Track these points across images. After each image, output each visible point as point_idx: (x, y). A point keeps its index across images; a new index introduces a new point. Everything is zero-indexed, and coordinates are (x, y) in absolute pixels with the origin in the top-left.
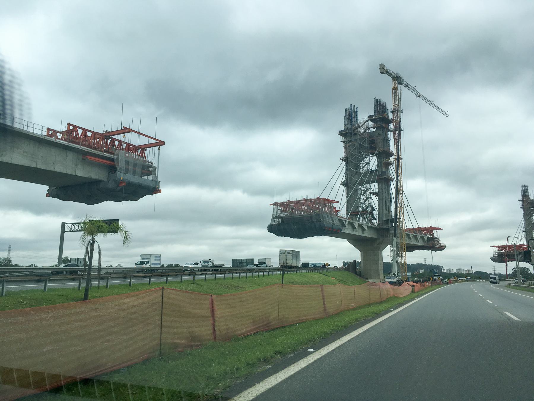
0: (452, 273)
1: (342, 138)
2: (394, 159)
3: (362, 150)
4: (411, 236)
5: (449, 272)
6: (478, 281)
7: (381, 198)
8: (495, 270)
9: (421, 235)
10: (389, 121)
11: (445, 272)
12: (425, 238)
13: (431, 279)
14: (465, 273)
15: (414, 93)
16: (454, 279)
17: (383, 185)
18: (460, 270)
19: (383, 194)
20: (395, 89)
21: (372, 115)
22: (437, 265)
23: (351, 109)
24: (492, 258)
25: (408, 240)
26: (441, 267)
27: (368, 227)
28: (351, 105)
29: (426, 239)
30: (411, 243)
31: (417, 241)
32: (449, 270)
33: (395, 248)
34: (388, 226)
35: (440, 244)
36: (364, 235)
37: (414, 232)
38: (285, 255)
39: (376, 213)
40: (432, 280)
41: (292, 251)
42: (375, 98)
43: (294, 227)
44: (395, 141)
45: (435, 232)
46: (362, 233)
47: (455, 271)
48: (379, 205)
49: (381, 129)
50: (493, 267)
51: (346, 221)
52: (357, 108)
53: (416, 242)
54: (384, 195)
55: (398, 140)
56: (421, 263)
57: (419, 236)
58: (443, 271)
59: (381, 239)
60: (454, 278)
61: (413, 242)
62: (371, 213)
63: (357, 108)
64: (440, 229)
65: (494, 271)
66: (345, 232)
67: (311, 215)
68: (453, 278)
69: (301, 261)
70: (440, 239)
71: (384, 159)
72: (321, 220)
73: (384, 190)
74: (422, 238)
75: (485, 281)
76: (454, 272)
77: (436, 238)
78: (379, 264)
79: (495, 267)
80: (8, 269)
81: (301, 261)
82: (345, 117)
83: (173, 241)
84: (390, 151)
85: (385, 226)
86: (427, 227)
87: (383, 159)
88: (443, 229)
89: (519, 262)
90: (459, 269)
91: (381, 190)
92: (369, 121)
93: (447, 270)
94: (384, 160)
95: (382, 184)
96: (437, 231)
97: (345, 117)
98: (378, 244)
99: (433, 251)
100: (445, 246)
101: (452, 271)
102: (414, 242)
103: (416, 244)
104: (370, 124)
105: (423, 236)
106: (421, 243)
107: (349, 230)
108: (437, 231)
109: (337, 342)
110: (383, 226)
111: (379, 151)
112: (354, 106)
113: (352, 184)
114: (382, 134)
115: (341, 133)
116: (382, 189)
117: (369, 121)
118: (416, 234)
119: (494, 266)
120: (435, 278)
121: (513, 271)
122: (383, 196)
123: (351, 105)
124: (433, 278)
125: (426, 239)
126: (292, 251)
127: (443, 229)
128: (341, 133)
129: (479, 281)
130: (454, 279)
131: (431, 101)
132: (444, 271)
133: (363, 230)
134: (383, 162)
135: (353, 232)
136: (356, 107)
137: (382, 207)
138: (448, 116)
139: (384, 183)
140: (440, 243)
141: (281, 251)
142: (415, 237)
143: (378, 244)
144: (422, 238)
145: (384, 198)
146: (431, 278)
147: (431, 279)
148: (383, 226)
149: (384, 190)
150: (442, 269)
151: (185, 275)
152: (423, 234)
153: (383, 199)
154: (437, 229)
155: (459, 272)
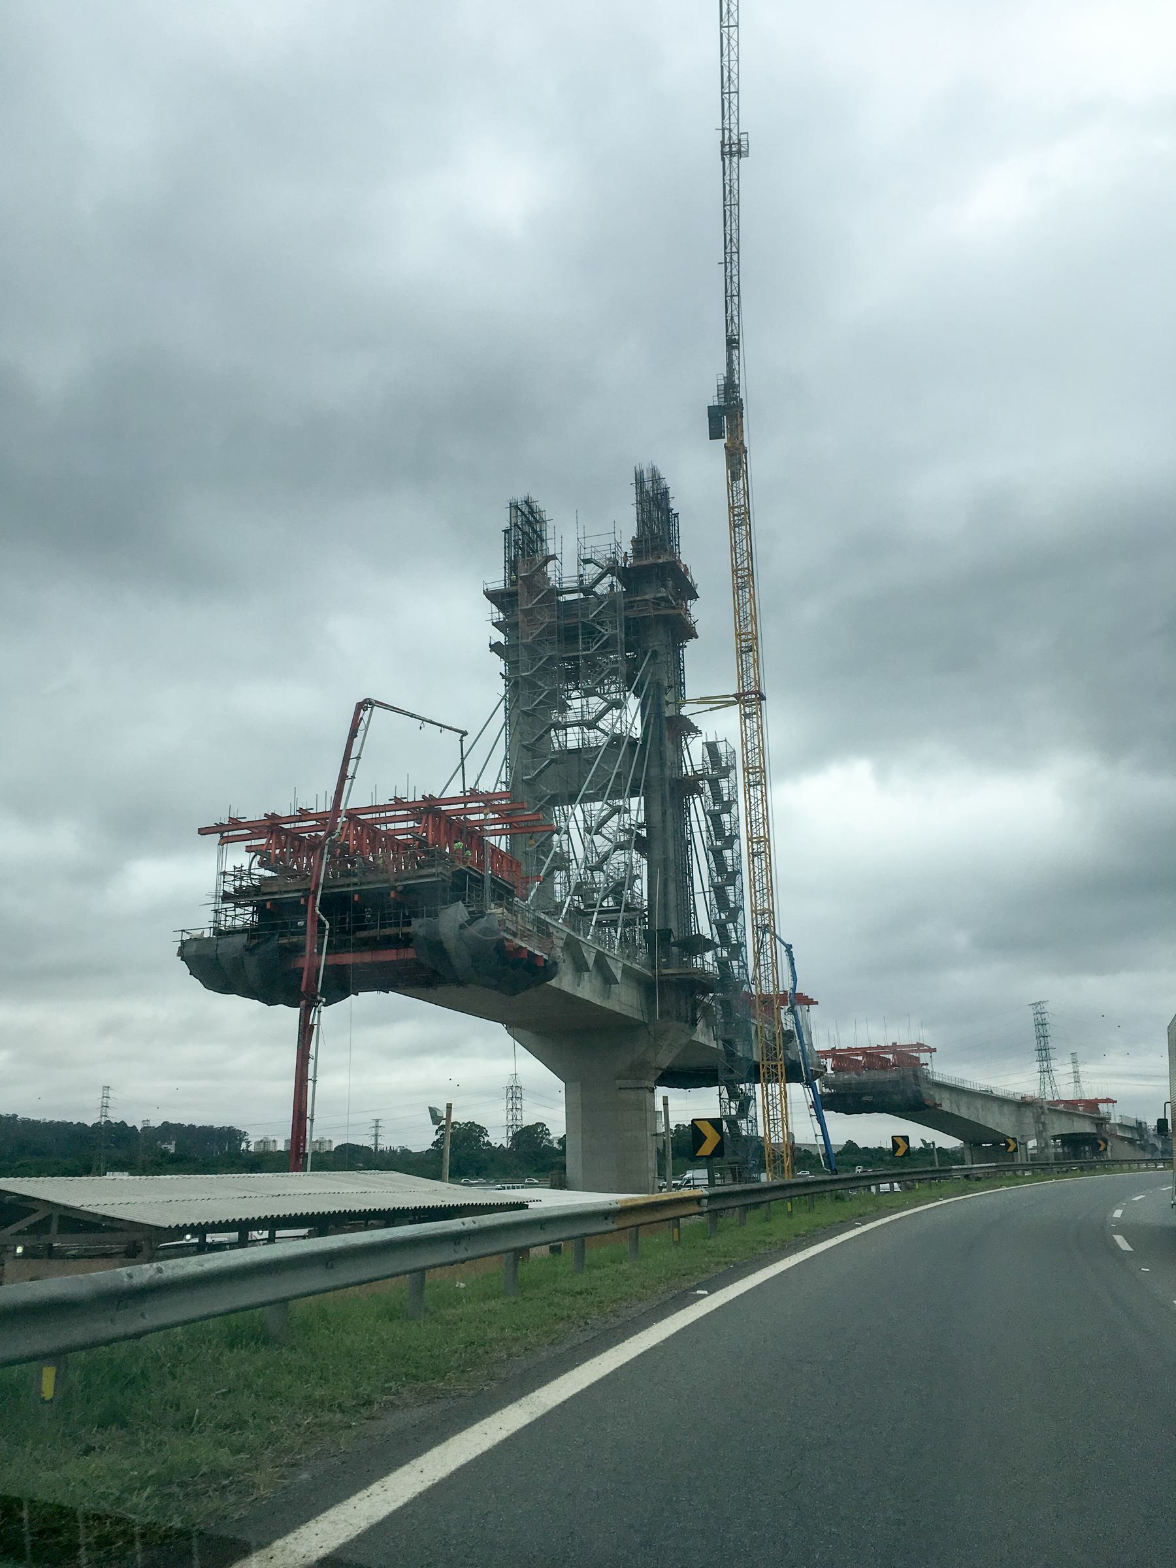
2: (733, 696)
5: (320, 1148)
8: (379, 1133)
11: (252, 1149)
13: (1100, 1145)
22: (230, 1128)
27: (626, 971)
32: (264, 1142)
50: (374, 1125)
56: (177, 1122)
58: (244, 1145)
76: (278, 1149)
79: (380, 1124)
80: (984, 1167)
82: (506, 531)
93: (258, 1143)
97: (506, 531)
101: (272, 1144)
109: (485, 1424)
119: (377, 1121)
121: (438, 1137)
133: (608, 979)
147: (1100, 1145)
150: (241, 1140)
151: (1121, 1162)
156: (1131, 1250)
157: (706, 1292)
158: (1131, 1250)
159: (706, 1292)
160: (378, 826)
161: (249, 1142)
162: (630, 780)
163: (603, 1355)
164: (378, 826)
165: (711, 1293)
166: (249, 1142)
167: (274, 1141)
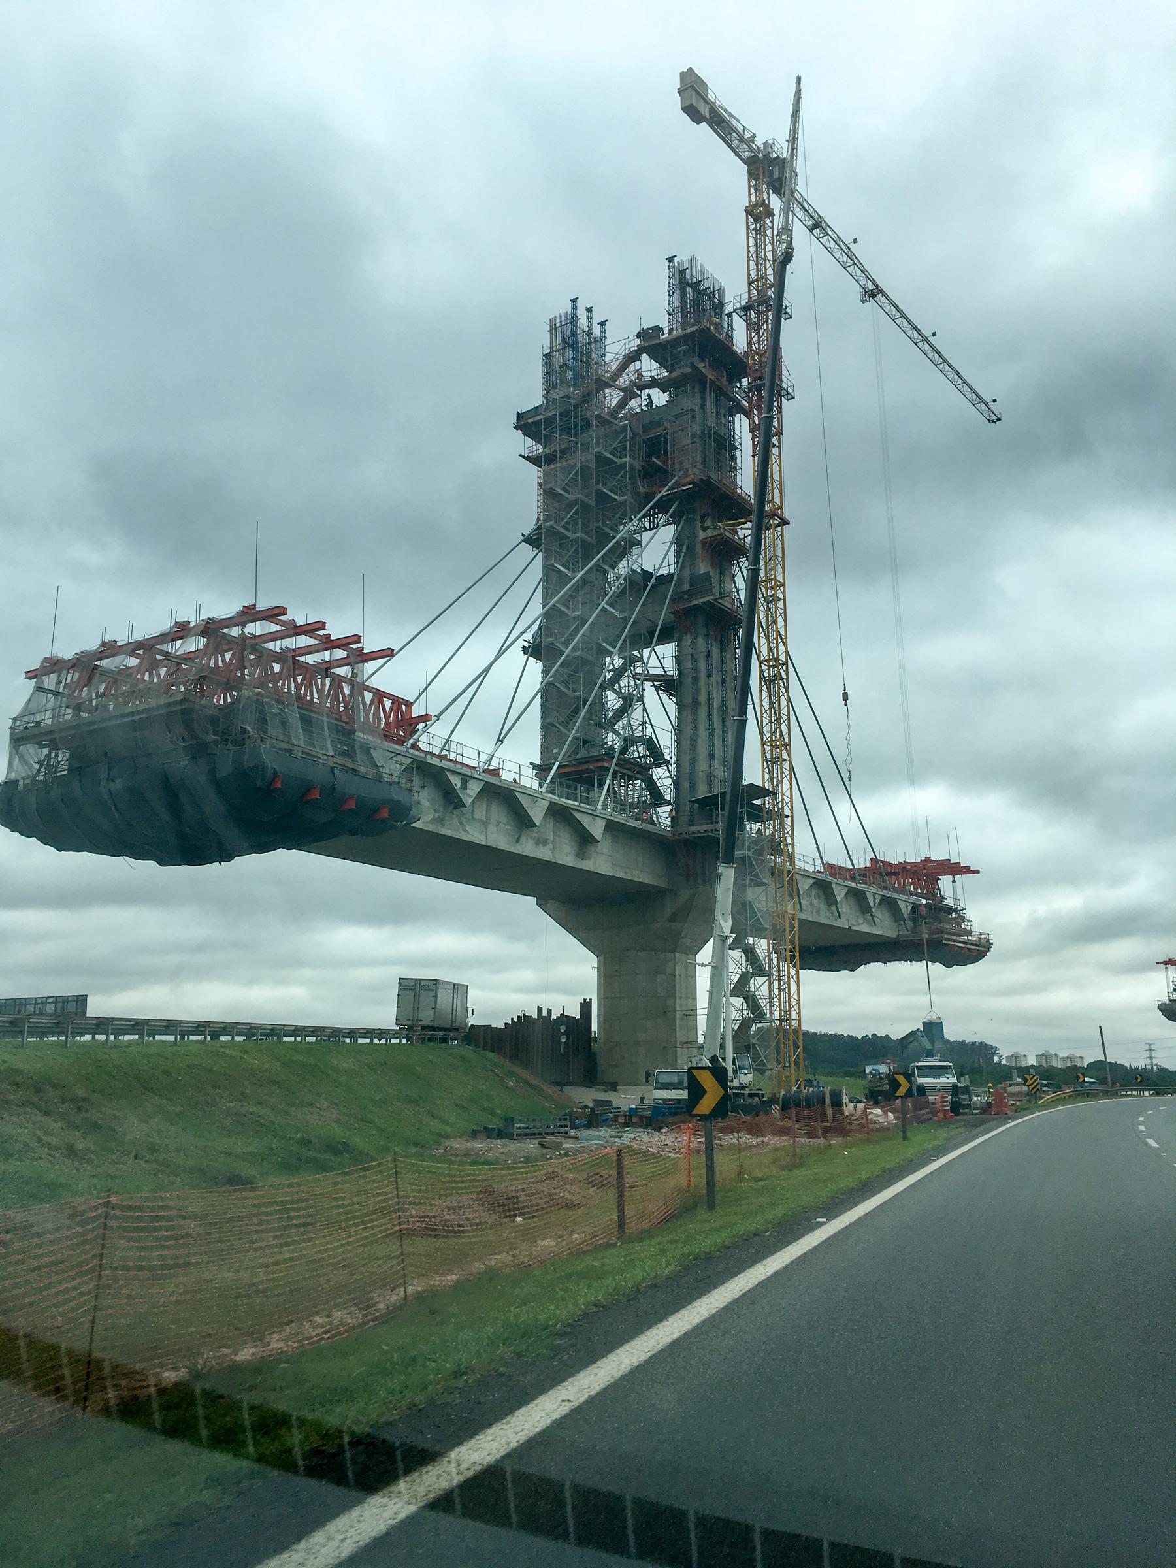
0: (1023, 1065)
1: (529, 445)
3: (610, 485)
4: (840, 894)
6: (1132, 1096)
7: (688, 700)
9: (884, 893)
10: (734, 366)
11: (1004, 1062)
12: (902, 905)
14: (1060, 1067)
15: (850, 269)
16: (1025, 1088)
17: (701, 641)
18: (1046, 1056)
19: (696, 680)
20: (758, 213)
21: (658, 329)
22: (981, 1043)
23: (574, 320)
24: (1165, 1004)
25: (823, 907)
26: (992, 1048)
28: (574, 301)
29: (905, 910)
30: (841, 923)
31: (868, 916)
32: (1015, 1057)
33: (726, 921)
34: (712, 827)
35: (969, 933)
36: (588, 865)
37: (853, 879)
38: (412, 993)
39: (662, 777)
40: (909, 1093)
41: (435, 982)
42: (671, 260)
43: (112, 786)
44: (753, 439)
45: (945, 883)
46: (577, 855)
47: (1032, 1061)
48: (679, 731)
49: (697, 390)
50: (1147, 1047)
51: (465, 779)
52: (603, 324)
53: (861, 920)
54: (702, 683)
55: (766, 436)
57: (873, 893)
58: (996, 1059)
59: (684, 895)
60: (1025, 1080)
61: (848, 919)
62: (640, 771)
63: (603, 324)
64: (967, 870)
65: (1151, 1058)
66: (464, 837)
67: (186, 705)
68: (1019, 1080)
69: (473, 1014)
70: (969, 914)
71: (708, 523)
72: (244, 731)
73: (702, 666)
74: (890, 904)
75: (1146, 1093)
76: (1030, 1064)
77: (949, 910)
78: (678, 1015)
79: (1153, 1047)
81: (473, 1014)
83: (200, 973)
84: (739, 491)
85: (700, 828)
86: (911, 860)
87: (703, 522)
88: (977, 871)
89: (1104, 1060)
90: (1043, 1055)
91: (689, 664)
92: (644, 357)
93: (1009, 1058)
94: (705, 529)
95: (696, 638)
96: (954, 882)
98: (673, 918)
99: (937, 968)
100: (988, 945)
102: (852, 921)
103: (864, 928)
104: (648, 366)
105: (895, 895)
106: (882, 927)
107: (492, 828)
108: (954, 882)
110: (693, 829)
111: (684, 481)
112: (589, 310)
113: (556, 639)
114: (697, 408)
115: (526, 424)
116: (695, 660)
117: (644, 357)
118: (862, 886)
119: (1150, 1045)
120: (920, 1080)
122: (698, 691)
123: (574, 301)
124: (910, 1081)
125: (905, 910)
126: (435, 982)
127: (977, 871)
128: (526, 424)
129: (1135, 1093)
130: (1025, 1088)
131: (927, 333)
132: (1000, 1060)
134: (702, 535)
135: (517, 841)
136: (596, 319)
137: (694, 740)
138: (999, 420)
139: (703, 631)
140: (969, 928)
141: (404, 982)
142: (857, 896)
143: (673, 918)
144: (890, 904)
145: (703, 698)
146: (901, 1079)
148: (693, 829)
149: (702, 666)
150: (993, 1054)
152: (896, 890)
153: (696, 703)
154: (955, 869)
155: (1044, 1065)
156: (753, 802)
157: (825, 1220)
158: (753, 802)
159: (825, 1220)
160: (226, 631)
161: (1001, 1056)
162: (671, 591)
163: (660, 1326)
164: (226, 631)
165: (829, 1220)
166: (1001, 1056)
167: (1025, 1056)
